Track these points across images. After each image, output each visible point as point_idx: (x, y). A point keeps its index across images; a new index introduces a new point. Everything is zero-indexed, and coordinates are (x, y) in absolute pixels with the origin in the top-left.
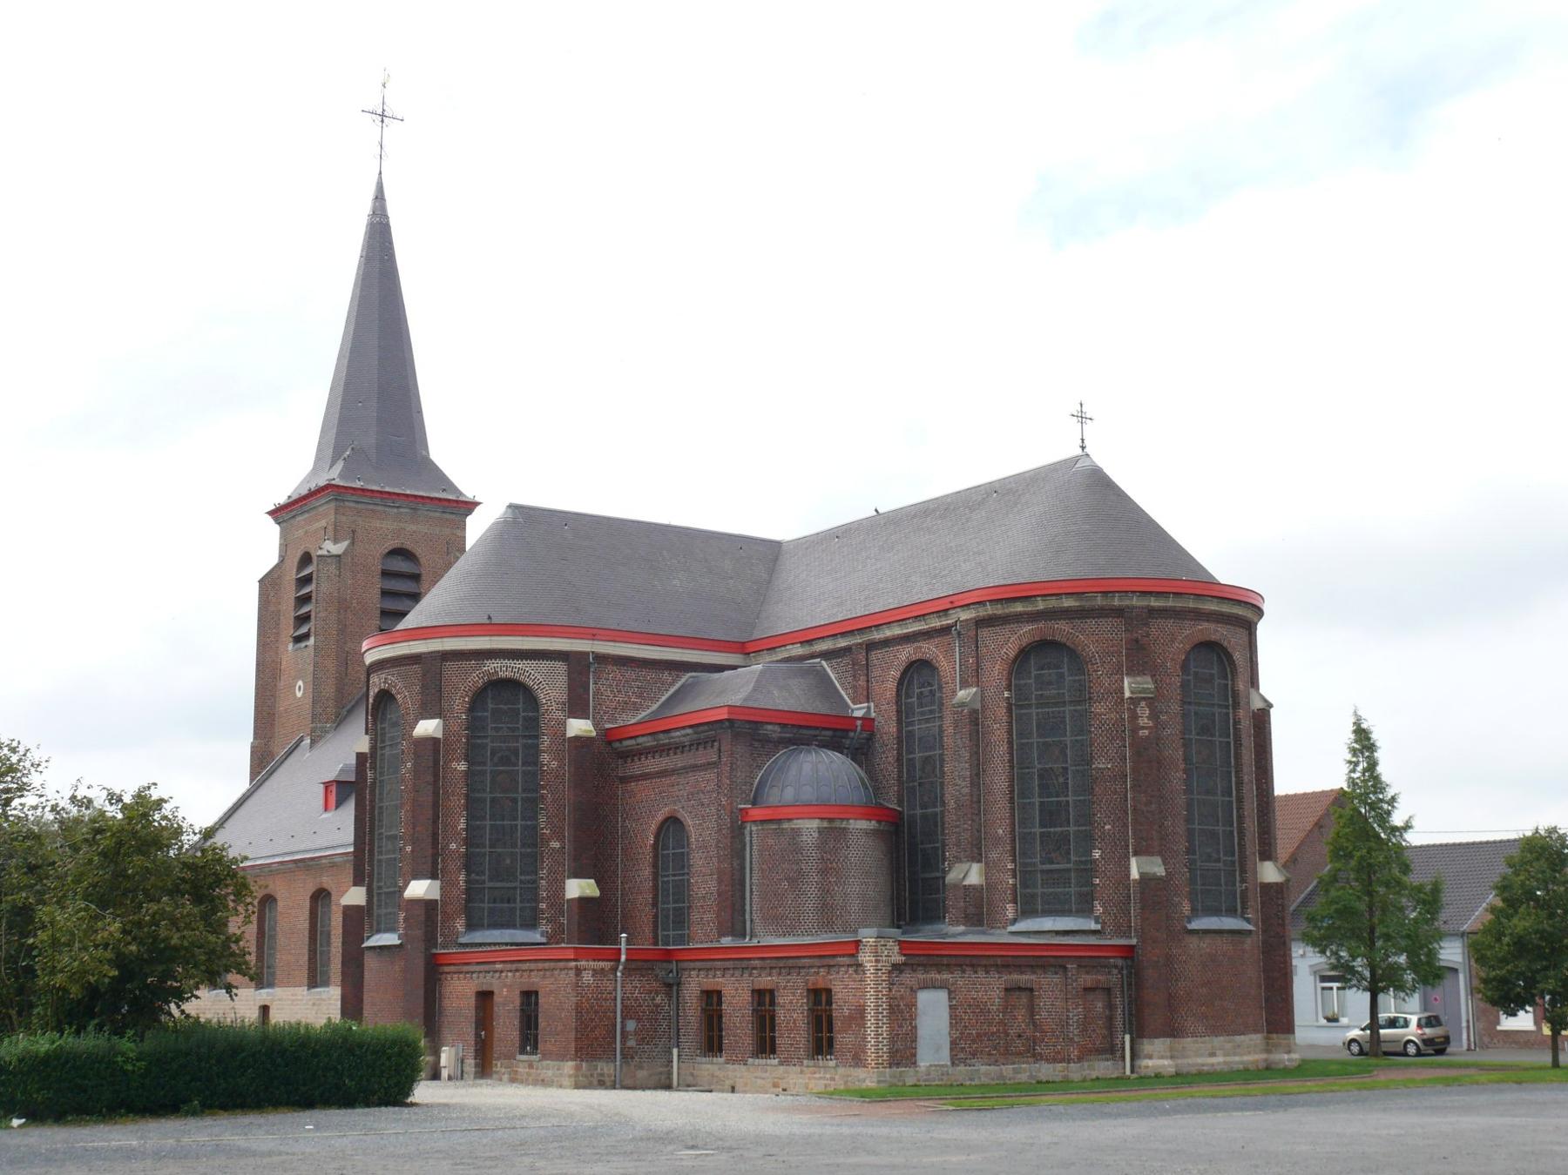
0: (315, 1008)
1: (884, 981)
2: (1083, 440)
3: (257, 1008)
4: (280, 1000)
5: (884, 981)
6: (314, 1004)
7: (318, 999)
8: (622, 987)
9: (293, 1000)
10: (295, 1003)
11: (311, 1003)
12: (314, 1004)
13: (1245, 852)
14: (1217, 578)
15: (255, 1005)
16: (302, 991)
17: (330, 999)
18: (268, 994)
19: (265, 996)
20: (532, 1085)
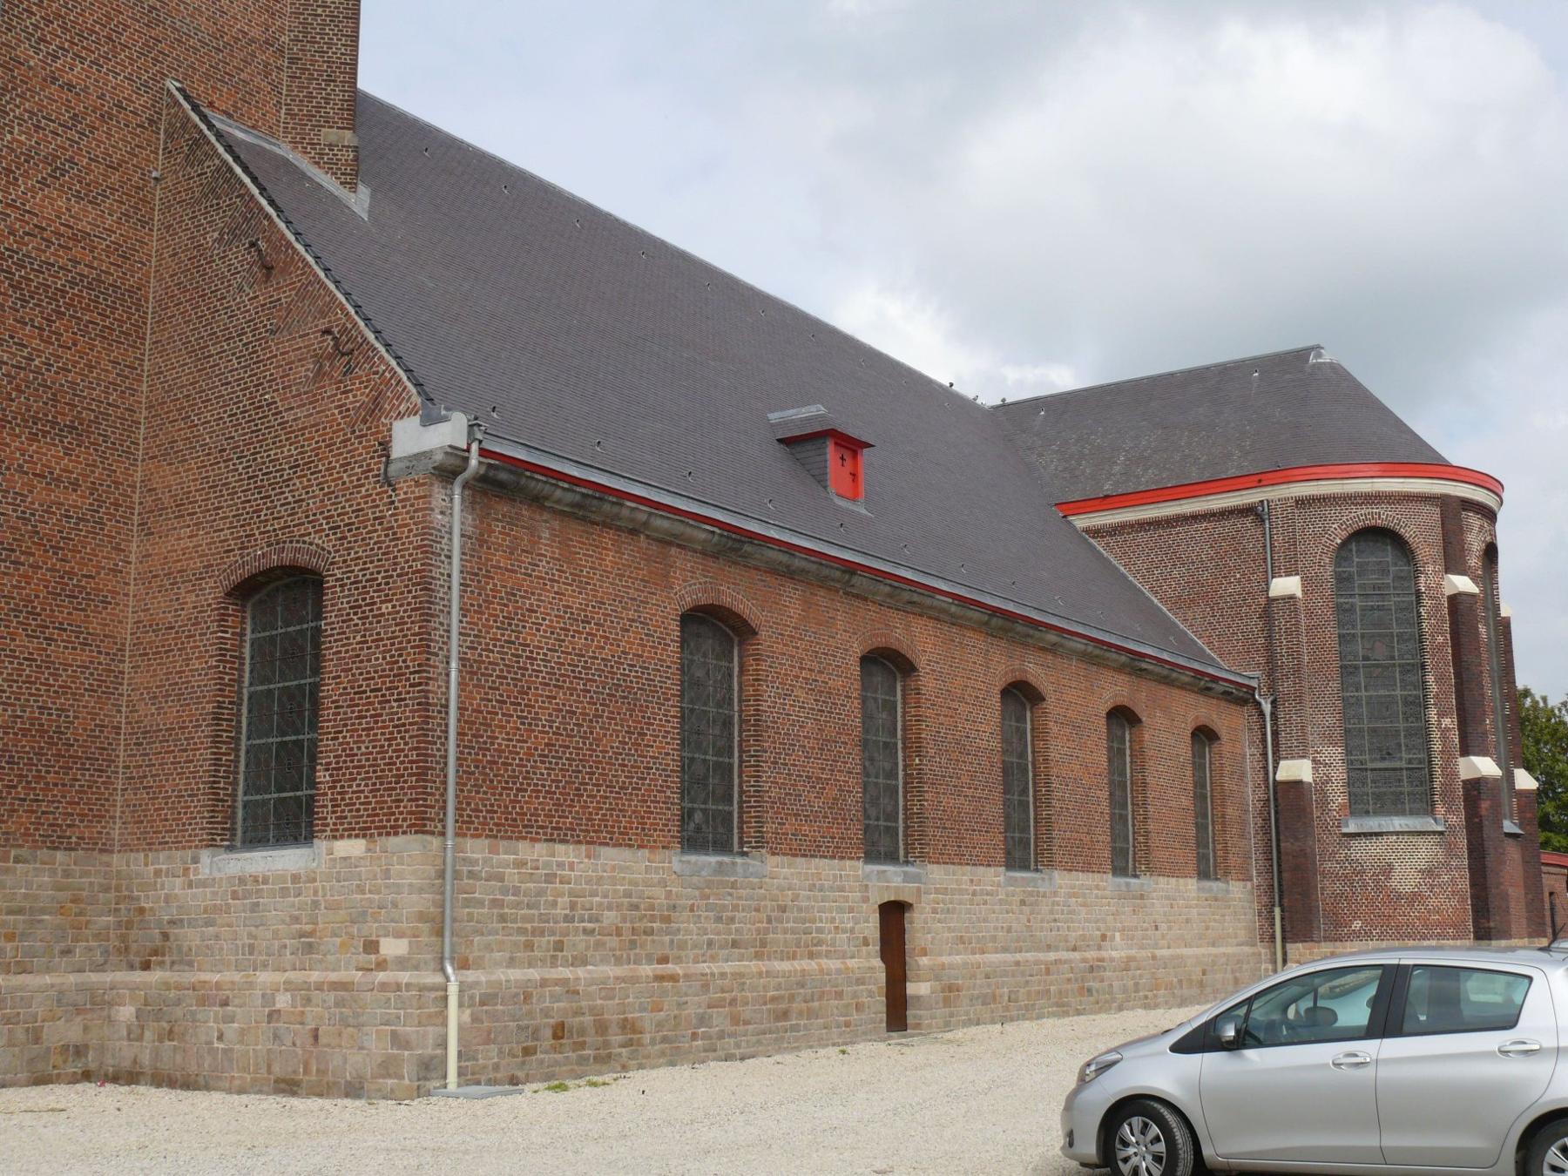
0: (1026, 909)
1: (675, 663)
2: (854, 475)
3: (877, 906)
4: (937, 891)
5: (675, 663)
6: (1023, 903)
7: (1031, 894)
8: (446, 732)
9: (974, 893)
10: (978, 898)
11: (1017, 899)
12: (1023, 903)
13: (530, 506)
14: (1447, 458)
15: (866, 900)
16: (995, 876)
17: (1055, 894)
18: (907, 878)
19: (897, 881)
20: (167, 1086)
